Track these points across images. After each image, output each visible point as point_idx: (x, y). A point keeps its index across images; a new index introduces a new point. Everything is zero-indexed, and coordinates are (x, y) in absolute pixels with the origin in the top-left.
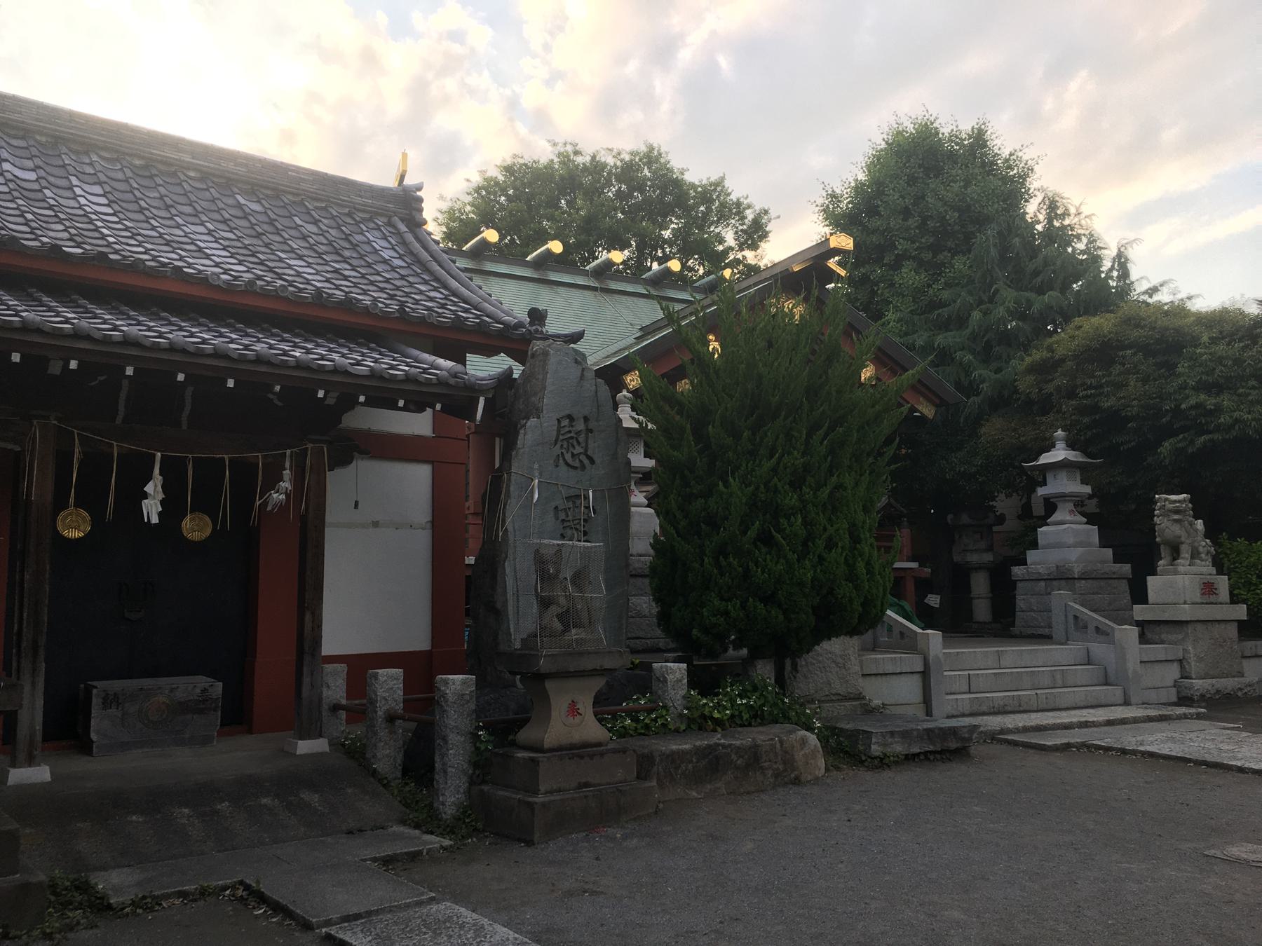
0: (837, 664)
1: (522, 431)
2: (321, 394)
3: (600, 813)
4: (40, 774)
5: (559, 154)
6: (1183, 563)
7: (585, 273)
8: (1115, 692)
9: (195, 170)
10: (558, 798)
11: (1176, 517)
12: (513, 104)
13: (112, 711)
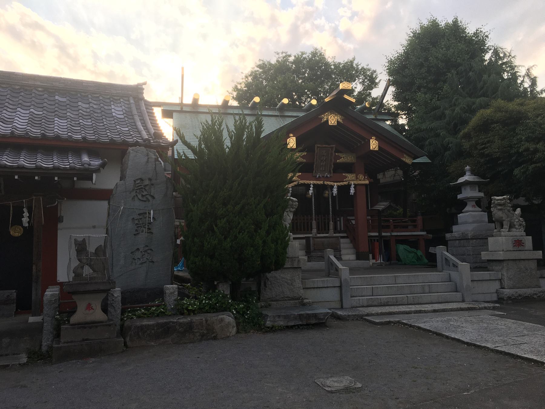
0: (288, 283)
6: (505, 231)
7: (275, 110)
8: (458, 295)
9: (41, 87)
11: (499, 207)
12: (335, 31)
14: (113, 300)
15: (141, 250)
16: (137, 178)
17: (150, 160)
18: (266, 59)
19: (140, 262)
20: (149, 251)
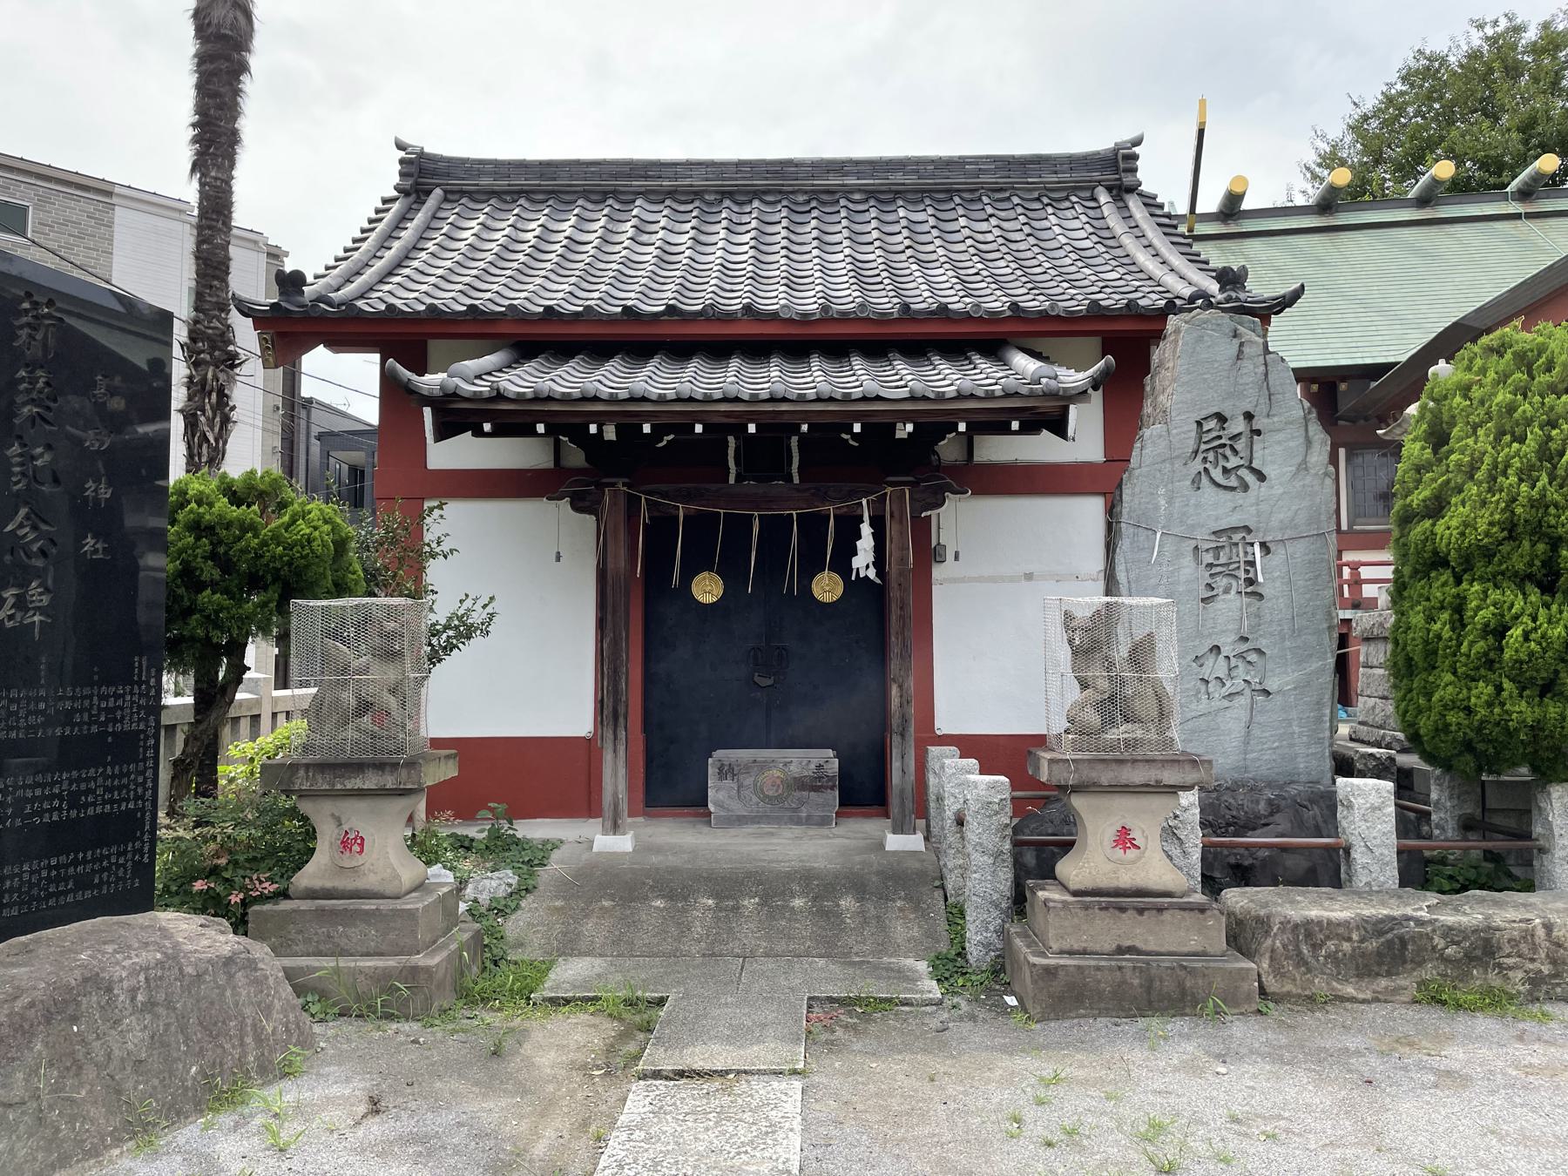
1: (1138, 445)
2: (593, 429)
3: (1155, 995)
4: (623, 843)
5: (1492, 40)
10: (1093, 963)
13: (728, 782)
14: (1176, 817)
15: (1226, 651)
16: (1204, 413)
17: (1246, 350)
18: (1437, 45)
19: (1225, 691)
20: (1253, 657)
